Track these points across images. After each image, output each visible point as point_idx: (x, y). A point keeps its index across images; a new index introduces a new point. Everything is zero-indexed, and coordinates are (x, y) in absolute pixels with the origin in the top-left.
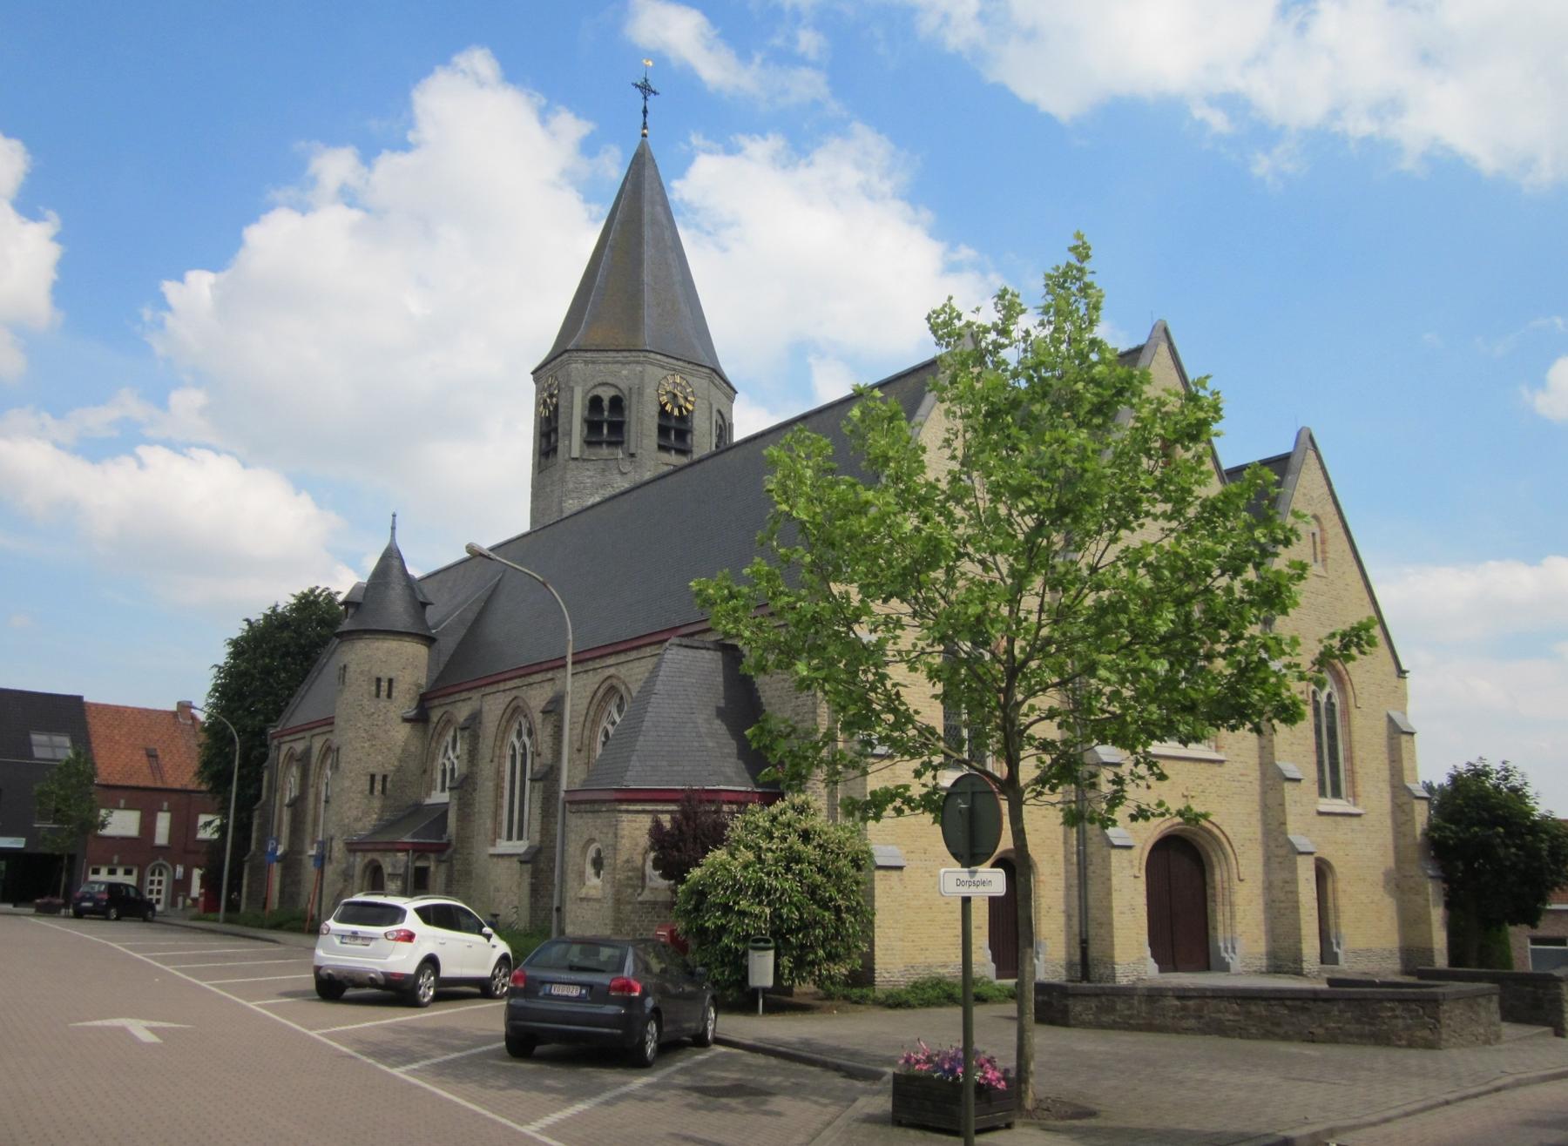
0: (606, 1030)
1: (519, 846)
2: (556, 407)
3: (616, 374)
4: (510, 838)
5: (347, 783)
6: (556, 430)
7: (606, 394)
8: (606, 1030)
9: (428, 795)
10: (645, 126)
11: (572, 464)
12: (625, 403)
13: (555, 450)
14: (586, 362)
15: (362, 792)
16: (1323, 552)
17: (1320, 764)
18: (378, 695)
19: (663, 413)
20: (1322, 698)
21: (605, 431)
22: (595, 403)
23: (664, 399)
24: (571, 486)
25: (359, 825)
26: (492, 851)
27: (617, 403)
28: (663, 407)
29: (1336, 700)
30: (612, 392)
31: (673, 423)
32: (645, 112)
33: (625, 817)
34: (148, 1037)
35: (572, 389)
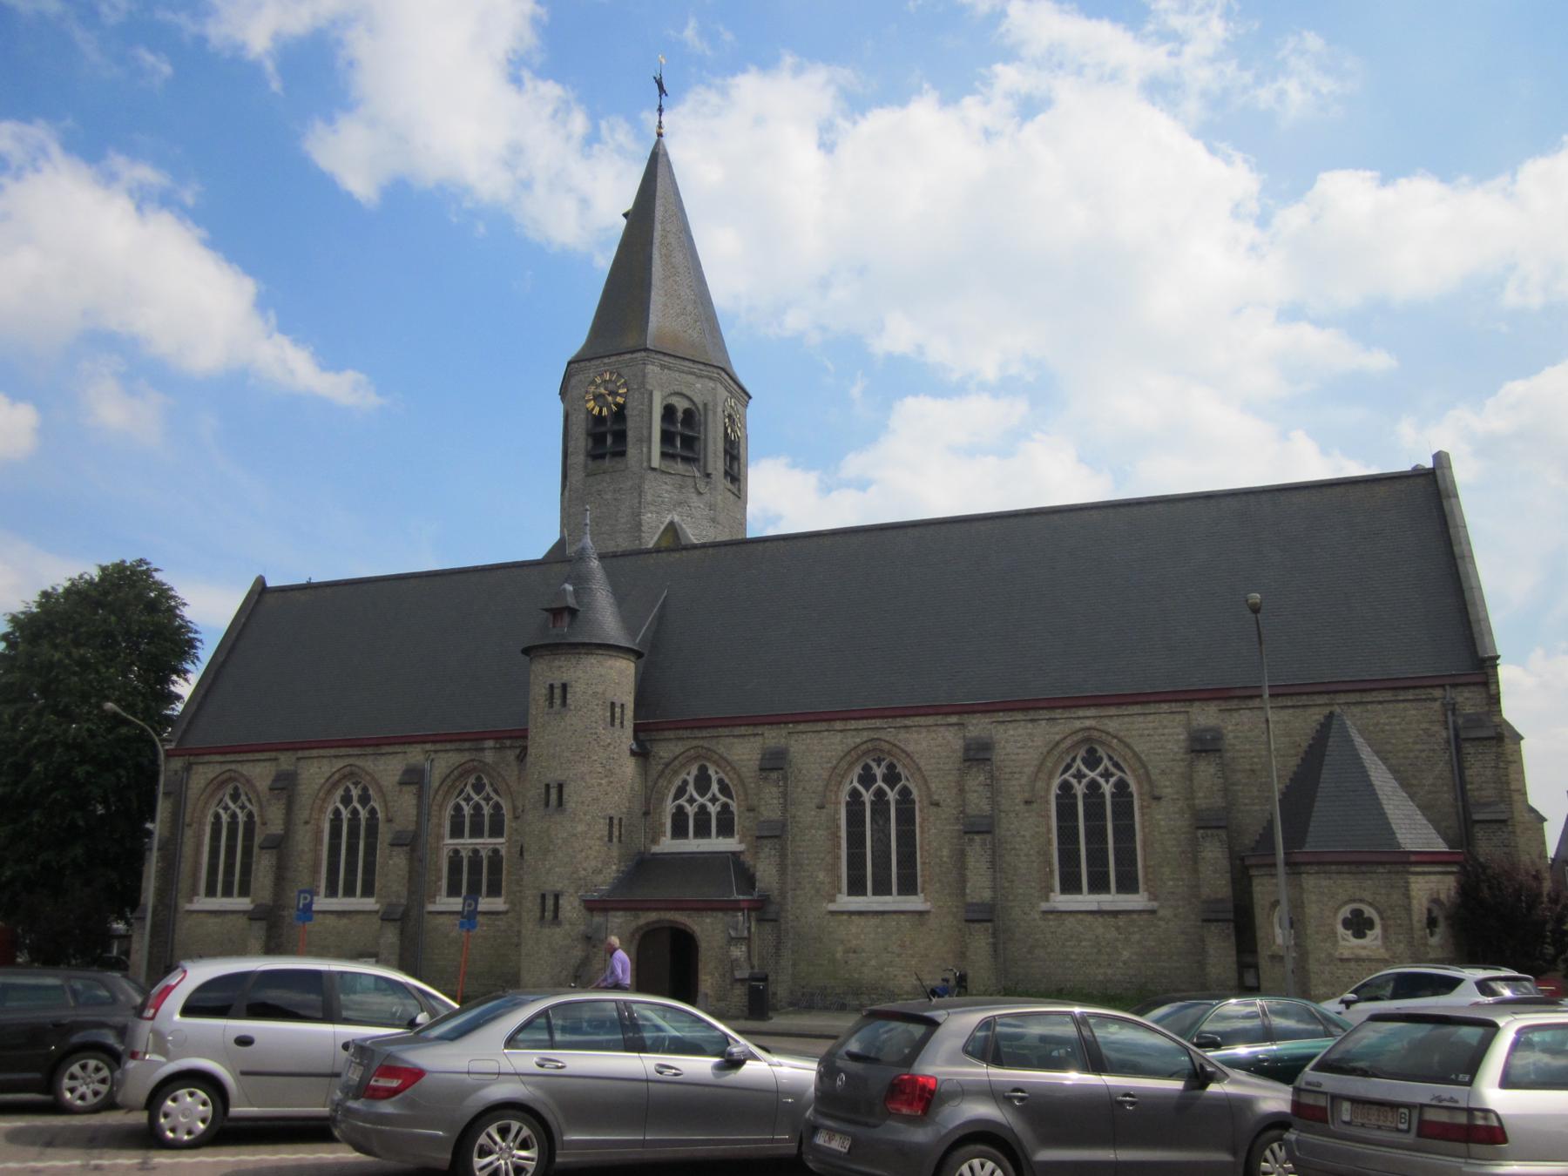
0: (1073, 1078)
1: (244, 903)
4: (211, 892)
5: (580, 828)
7: (681, 405)
9: (655, 841)
11: (651, 475)
14: (663, 367)
15: (600, 839)
18: (612, 724)
21: (679, 444)
22: (669, 411)
24: (649, 498)
25: (600, 878)
33: (1412, 879)
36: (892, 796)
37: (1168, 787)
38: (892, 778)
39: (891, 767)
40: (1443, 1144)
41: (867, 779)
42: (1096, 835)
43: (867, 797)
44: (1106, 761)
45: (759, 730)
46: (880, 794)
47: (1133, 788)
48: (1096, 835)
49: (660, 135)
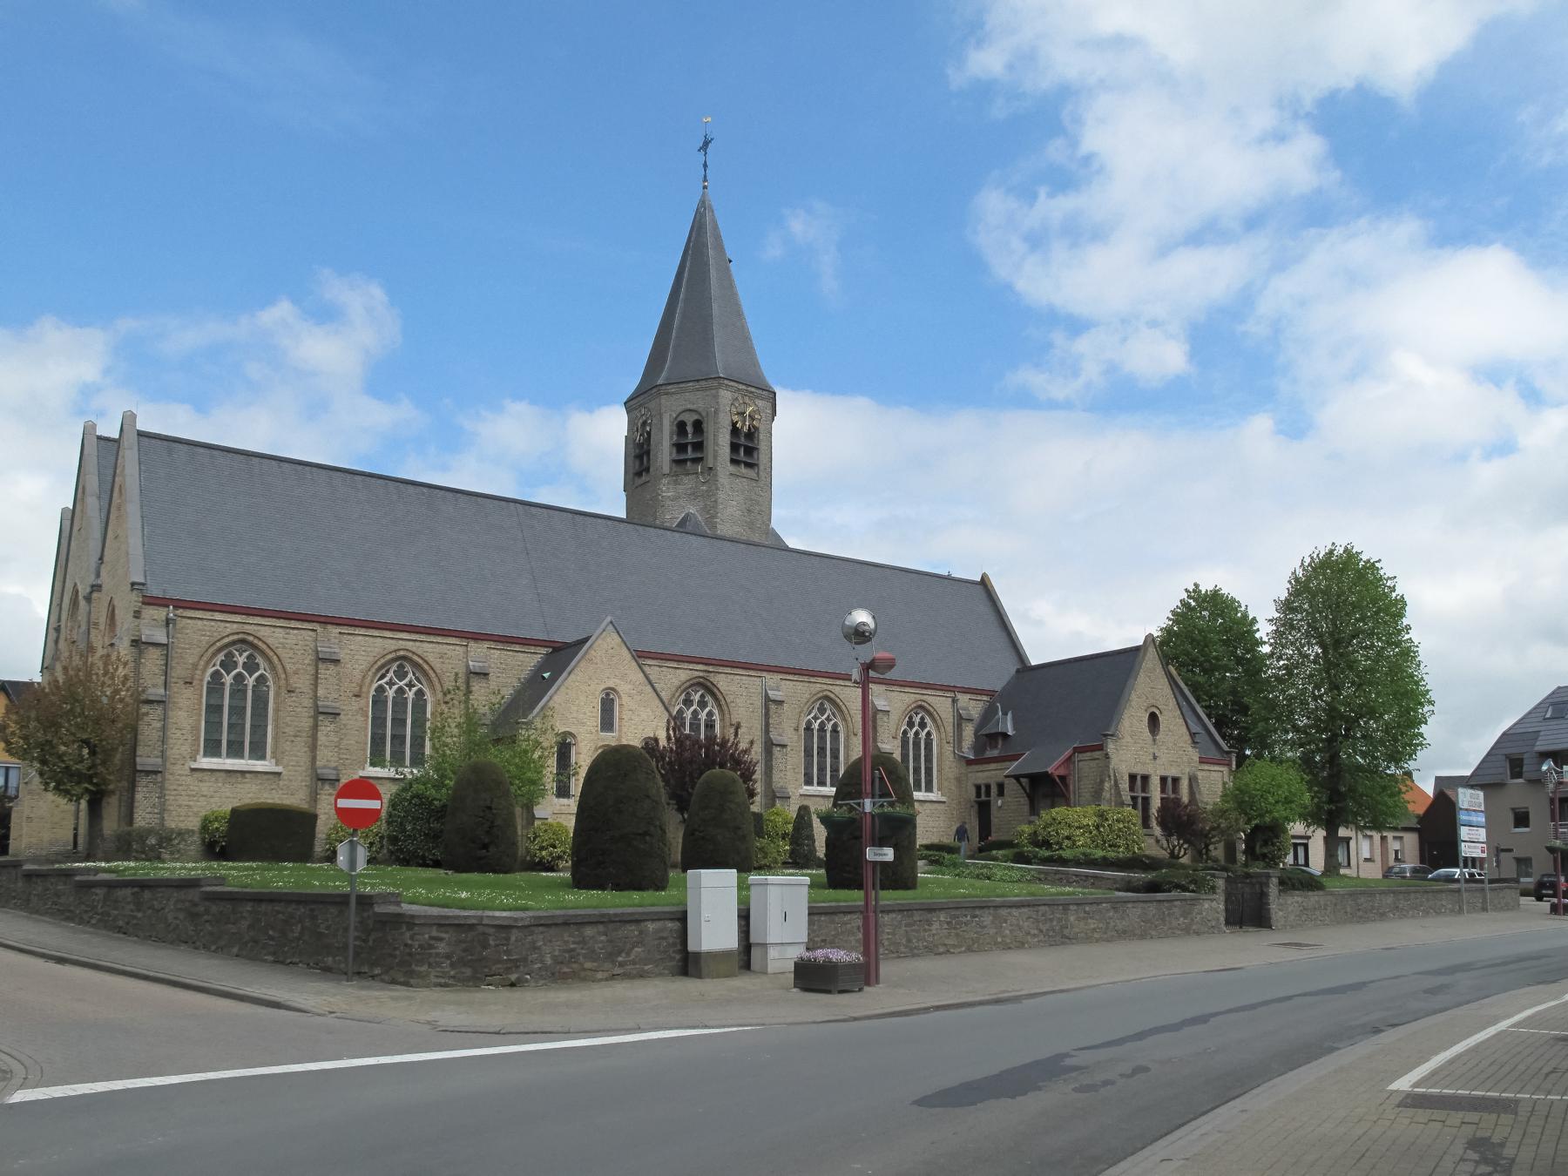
0: (505, 914)
2: (649, 433)
6: (648, 453)
7: (689, 419)
8: (505, 914)
10: (705, 180)
13: (647, 470)
17: (875, 728)
19: (735, 431)
20: (703, 716)
22: (681, 426)
23: (736, 418)
27: (698, 426)
28: (734, 424)
29: (716, 717)
30: (696, 417)
31: (742, 440)
32: (705, 166)
34: (1394, 1086)
35: (661, 415)
36: (250, 681)
38: (251, 666)
41: (911, 724)
42: (237, 711)
43: (228, 679)
46: (239, 678)
48: (237, 711)
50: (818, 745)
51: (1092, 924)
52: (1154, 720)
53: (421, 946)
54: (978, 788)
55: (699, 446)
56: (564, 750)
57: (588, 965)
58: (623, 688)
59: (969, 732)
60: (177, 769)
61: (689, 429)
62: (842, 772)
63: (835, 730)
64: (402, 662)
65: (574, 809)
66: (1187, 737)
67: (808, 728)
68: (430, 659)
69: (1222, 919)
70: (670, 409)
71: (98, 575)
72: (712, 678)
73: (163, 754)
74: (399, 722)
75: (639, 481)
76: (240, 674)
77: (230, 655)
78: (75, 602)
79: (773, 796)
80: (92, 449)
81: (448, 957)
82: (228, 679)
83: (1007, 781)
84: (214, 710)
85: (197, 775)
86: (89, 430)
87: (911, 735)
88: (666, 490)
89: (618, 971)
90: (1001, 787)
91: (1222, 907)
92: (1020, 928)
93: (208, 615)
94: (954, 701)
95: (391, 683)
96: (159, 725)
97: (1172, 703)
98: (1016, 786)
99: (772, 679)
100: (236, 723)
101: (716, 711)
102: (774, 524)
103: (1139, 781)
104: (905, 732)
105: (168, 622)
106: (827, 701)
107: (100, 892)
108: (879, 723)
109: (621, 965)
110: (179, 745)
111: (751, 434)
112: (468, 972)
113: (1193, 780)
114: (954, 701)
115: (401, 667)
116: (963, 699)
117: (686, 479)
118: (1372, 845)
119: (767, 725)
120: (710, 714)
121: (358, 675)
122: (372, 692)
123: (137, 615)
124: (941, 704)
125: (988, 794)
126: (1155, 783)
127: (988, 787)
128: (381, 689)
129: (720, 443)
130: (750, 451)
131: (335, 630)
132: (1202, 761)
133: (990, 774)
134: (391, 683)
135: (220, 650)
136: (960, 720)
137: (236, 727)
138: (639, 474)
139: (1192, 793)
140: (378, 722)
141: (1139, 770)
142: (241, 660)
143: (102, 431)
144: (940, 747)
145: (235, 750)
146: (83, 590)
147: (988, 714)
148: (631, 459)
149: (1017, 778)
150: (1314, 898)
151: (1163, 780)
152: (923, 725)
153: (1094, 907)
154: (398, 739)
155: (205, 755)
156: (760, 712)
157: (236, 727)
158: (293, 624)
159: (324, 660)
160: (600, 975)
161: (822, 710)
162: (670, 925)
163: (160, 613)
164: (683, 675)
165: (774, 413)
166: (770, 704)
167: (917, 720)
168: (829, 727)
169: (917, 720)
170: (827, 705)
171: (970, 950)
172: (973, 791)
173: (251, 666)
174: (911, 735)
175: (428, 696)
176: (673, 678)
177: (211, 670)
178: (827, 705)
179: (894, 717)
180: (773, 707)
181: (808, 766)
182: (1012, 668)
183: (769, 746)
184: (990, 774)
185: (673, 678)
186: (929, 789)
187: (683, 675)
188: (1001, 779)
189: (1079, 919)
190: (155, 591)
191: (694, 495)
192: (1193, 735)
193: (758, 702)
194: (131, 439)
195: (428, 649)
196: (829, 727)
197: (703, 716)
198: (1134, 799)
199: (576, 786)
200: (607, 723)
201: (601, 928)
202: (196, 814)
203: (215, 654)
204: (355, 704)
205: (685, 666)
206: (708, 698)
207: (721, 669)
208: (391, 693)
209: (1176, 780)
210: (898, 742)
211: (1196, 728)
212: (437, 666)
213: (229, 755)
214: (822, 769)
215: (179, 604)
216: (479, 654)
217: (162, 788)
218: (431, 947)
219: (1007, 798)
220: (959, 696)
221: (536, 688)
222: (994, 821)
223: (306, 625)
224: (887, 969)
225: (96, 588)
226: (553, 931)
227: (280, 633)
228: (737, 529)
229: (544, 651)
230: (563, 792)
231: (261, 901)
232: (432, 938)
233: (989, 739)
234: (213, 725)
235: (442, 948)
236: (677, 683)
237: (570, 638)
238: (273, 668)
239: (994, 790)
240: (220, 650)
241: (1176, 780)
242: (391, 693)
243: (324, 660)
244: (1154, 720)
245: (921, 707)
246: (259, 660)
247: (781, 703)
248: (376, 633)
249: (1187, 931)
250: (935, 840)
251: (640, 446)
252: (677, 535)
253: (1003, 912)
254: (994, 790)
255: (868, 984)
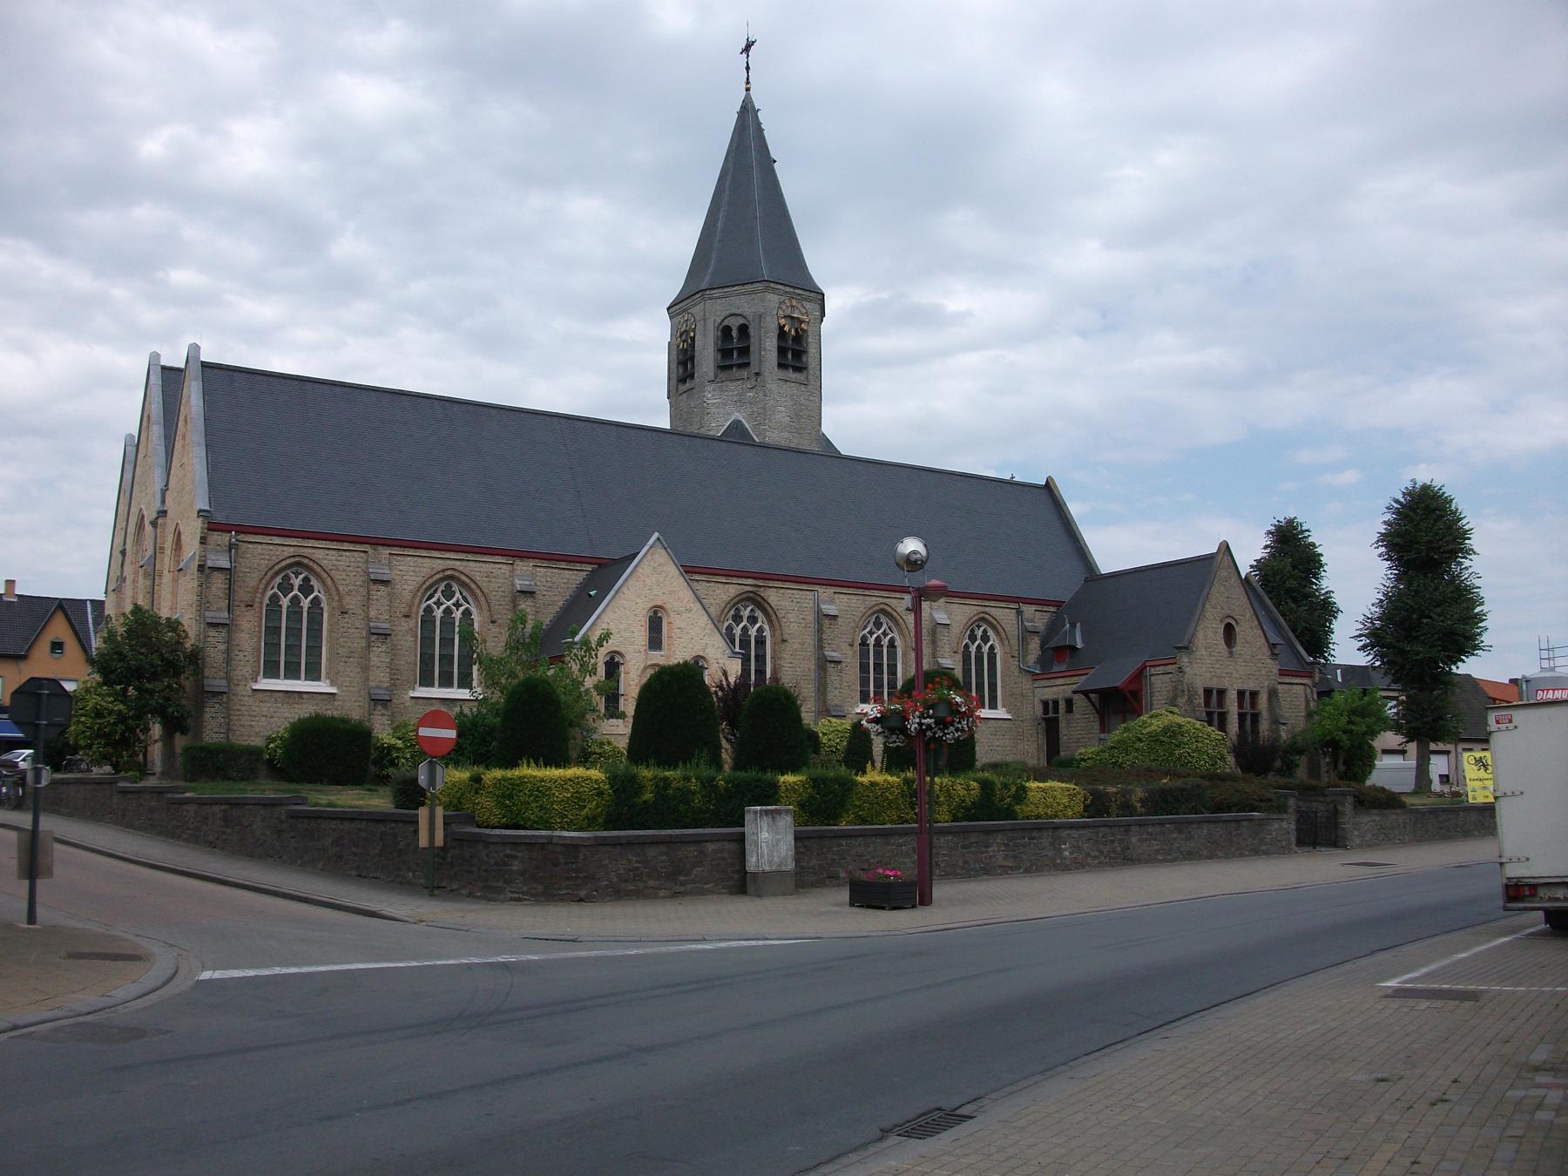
2: (693, 339)
3: (743, 304)
6: (692, 359)
7: (734, 323)
12: (752, 331)
13: (692, 376)
16: (273, 631)
19: (782, 334)
20: (753, 632)
22: (726, 331)
23: (783, 321)
26: (256, 687)
27: (744, 330)
28: (781, 328)
29: (767, 633)
30: (742, 321)
36: (306, 603)
37: (353, 603)
38: (306, 589)
39: (306, 579)
40: (302, 860)
41: (973, 638)
42: (294, 633)
43: (285, 602)
44: (458, 595)
45: (816, 588)
46: (295, 601)
47: (324, 605)
48: (294, 633)
49: (748, 90)
50: (873, 665)
51: (1156, 845)
52: (1229, 632)
53: (496, 864)
54: (1045, 704)
55: (745, 351)
56: (613, 667)
57: (651, 883)
58: (671, 604)
59: (1034, 645)
60: (240, 690)
61: (735, 333)
62: (900, 684)
63: (892, 644)
64: (449, 580)
65: (628, 731)
66: (1266, 649)
67: (864, 643)
68: (477, 578)
69: (1293, 839)
70: (714, 312)
71: (163, 502)
72: (762, 592)
73: (228, 678)
74: (447, 642)
75: (683, 388)
76: (296, 596)
77: (287, 578)
78: (140, 526)
79: (825, 711)
80: (156, 379)
81: (522, 873)
82: (285, 602)
83: (1076, 697)
84: (273, 631)
85: (260, 695)
86: (155, 357)
87: (973, 649)
88: (711, 396)
89: (679, 889)
90: (1069, 703)
91: (1293, 826)
92: (1080, 849)
93: (267, 539)
94: (1019, 612)
95: (438, 603)
96: (223, 647)
97: (1249, 614)
98: (1085, 702)
99: (825, 592)
100: (292, 646)
101: (766, 627)
102: (825, 429)
103: (1215, 696)
104: (967, 646)
105: (231, 546)
106: (882, 614)
107: (191, 808)
108: (939, 637)
109: (683, 884)
110: (243, 669)
111: (800, 337)
112: (540, 888)
113: (1273, 693)
114: (1019, 612)
115: (449, 586)
116: (1028, 610)
117: (732, 386)
118: (394, 653)
119: (820, 640)
120: (760, 630)
121: (407, 596)
122: (421, 613)
123: (203, 541)
124: (1004, 615)
125: (1056, 710)
126: (1232, 696)
127: (1056, 703)
128: (429, 610)
129: (767, 347)
130: (799, 354)
131: (386, 551)
132: (1282, 673)
133: (1058, 689)
134: (438, 603)
135: (277, 573)
136: (1026, 634)
137: (293, 649)
138: (682, 380)
139: (774, 670)
140: (427, 641)
141: (1215, 684)
142: (297, 582)
143: (166, 361)
144: (1004, 662)
145: (292, 672)
146: (150, 515)
147: (1054, 627)
148: (674, 365)
149: (1086, 693)
150: (1394, 817)
151: (1241, 694)
152: (985, 638)
153: (1158, 829)
154: (446, 659)
155: (265, 676)
156: (813, 627)
157: (293, 649)
158: (346, 546)
159: (375, 581)
160: (662, 893)
161: (878, 625)
162: (727, 846)
163: (222, 539)
164: (731, 590)
165: (823, 314)
166: (824, 620)
167: (979, 633)
168: (885, 642)
169: (979, 633)
170: (883, 619)
171: (1027, 871)
172: (1039, 709)
173: (306, 589)
174: (973, 649)
175: (475, 616)
176: (722, 593)
177: (270, 593)
178: (883, 619)
179: (956, 629)
180: (826, 622)
181: (864, 682)
182: (1079, 577)
183: (823, 663)
184: (1058, 689)
185: (722, 593)
186: (993, 706)
187: (731, 590)
188: (1069, 695)
189: (1141, 840)
190: (219, 518)
191: (740, 402)
192: (1273, 646)
193: (811, 618)
194: (195, 371)
195: (476, 568)
196: (885, 642)
197: (753, 632)
198: (1209, 714)
199: (628, 706)
200: (655, 642)
201: (663, 848)
202: (257, 734)
203: (273, 578)
204: (405, 625)
205: (735, 580)
206: (759, 614)
207: (771, 584)
208: (438, 613)
209: (1254, 694)
210: (959, 657)
211: (1274, 639)
212: (484, 585)
213: (286, 677)
214: (879, 685)
215: (242, 529)
216: (524, 574)
217: (228, 709)
218: (506, 864)
219: (1077, 715)
220: (1025, 608)
221: (582, 605)
222: (1063, 739)
223: (358, 547)
224: (940, 891)
225: (163, 513)
226: (618, 849)
227: (333, 555)
228: (786, 435)
229: (589, 568)
230: (613, 711)
231: (343, 819)
232: (507, 856)
233: (1057, 655)
234: (272, 647)
235: (516, 866)
236: (726, 598)
237: (615, 553)
238: (327, 591)
239: (1062, 706)
240: (442, 579)
241: (1254, 694)
242: (438, 613)
243: (375, 581)
244: (1229, 632)
245: (983, 619)
246: (314, 582)
247: (835, 617)
248: (424, 553)
249: (1256, 852)
250: (997, 758)
251: (684, 351)
252: (724, 445)
253: (1064, 833)
254: (1062, 706)
255: (922, 903)
